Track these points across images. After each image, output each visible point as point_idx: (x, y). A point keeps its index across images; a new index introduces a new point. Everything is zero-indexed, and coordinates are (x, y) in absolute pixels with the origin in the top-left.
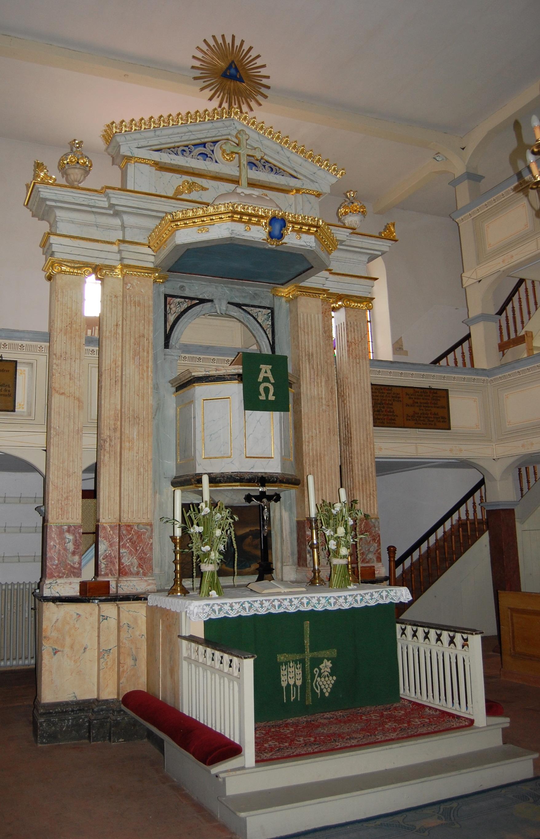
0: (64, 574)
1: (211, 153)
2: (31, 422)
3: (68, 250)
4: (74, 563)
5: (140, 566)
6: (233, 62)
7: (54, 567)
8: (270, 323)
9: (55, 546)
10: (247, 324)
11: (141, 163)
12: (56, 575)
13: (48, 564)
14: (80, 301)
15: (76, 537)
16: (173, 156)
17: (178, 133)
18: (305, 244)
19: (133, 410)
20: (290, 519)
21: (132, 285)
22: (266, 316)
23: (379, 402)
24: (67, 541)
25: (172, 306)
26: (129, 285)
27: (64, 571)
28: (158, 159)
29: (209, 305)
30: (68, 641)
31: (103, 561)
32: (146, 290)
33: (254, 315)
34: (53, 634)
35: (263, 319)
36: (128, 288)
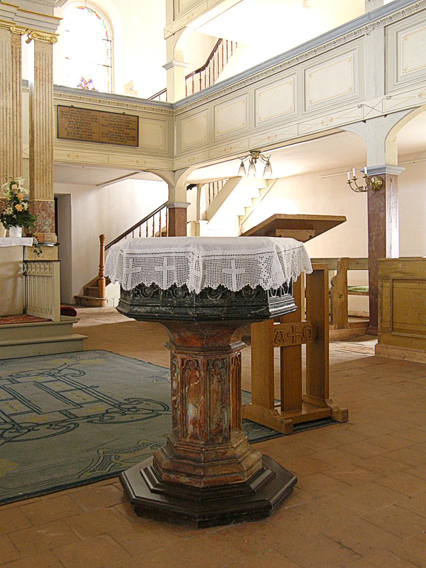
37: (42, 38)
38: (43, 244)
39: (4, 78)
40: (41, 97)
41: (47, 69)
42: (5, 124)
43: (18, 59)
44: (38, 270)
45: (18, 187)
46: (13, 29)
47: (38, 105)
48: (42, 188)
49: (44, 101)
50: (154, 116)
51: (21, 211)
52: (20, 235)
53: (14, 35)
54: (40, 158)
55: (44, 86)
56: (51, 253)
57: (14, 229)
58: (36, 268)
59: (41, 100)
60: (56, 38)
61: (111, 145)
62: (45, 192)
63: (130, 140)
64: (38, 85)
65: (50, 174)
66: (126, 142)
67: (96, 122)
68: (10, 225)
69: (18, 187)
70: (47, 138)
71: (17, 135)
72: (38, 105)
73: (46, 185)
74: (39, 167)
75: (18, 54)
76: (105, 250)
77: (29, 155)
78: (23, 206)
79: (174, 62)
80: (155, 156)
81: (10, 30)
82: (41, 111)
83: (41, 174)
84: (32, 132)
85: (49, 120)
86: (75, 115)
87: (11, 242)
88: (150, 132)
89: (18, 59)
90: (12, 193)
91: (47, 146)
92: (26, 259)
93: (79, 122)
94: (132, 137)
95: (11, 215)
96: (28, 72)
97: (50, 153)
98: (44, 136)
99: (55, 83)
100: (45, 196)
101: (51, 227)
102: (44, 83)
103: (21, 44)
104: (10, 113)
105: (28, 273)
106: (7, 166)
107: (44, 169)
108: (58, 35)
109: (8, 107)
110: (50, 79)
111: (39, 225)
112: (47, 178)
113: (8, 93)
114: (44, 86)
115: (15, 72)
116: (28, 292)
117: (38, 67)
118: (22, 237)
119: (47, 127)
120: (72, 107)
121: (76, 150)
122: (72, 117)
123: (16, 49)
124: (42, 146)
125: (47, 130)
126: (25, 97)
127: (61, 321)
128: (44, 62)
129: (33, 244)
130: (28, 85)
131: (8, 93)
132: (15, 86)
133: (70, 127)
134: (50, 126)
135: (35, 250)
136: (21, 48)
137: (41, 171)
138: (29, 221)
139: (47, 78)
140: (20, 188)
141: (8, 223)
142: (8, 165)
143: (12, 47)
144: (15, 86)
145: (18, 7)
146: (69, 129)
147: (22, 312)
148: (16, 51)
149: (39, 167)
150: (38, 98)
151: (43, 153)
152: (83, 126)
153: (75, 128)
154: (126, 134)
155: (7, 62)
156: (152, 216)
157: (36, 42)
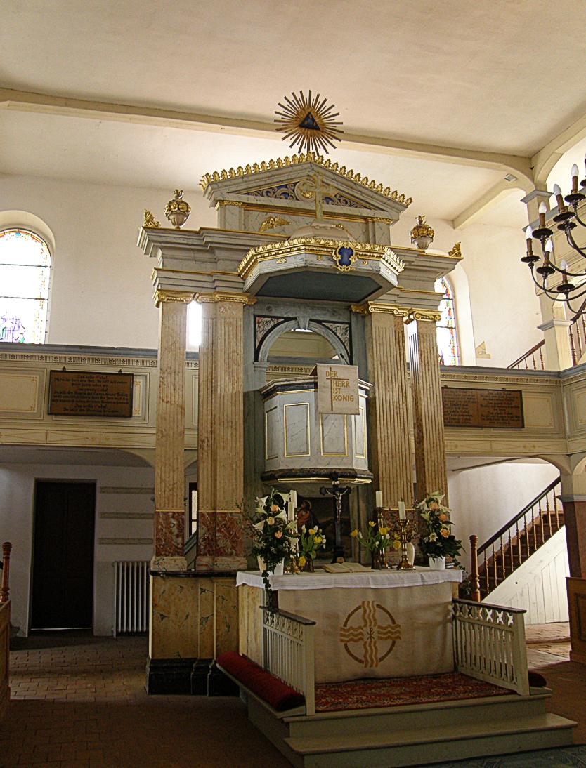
2: (146, 425)
3: (171, 282)
4: (178, 544)
5: (233, 547)
6: (310, 113)
10: (327, 338)
14: (212, 324)
15: (179, 522)
16: (259, 198)
17: (263, 178)
18: (371, 269)
19: (227, 416)
20: (367, 509)
22: (344, 331)
23: (455, 403)
29: (293, 322)
30: (173, 608)
31: (203, 543)
33: (334, 330)
34: (161, 602)
40: (428, 383)
50: (539, 389)
54: (431, 457)
59: (428, 388)
61: (492, 429)
63: (513, 420)
64: (424, 371)
65: (443, 475)
66: (509, 423)
67: (473, 402)
71: (405, 432)
75: (401, 339)
76: (478, 555)
79: (555, 322)
80: (543, 438)
82: (429, 401)
85: (433, 406)
88: (535, 408)
89: (401, 345)
91: (438, 441)
94: (516, 417)
97: (442, 450)
108: (441, 312)
109: (395, 400)
112: (440, 482)
115: (399, 360)
119: (437, 419)
124: (432, 443)
125: (437, 424)
127: (531, 695)
137: (433, 473)
147: (452, 669)
150: (425, 386)
152: (459, 408)
154: (509, 414)
155: (392, 349)
156: (529, 509)
157: (421, 325)
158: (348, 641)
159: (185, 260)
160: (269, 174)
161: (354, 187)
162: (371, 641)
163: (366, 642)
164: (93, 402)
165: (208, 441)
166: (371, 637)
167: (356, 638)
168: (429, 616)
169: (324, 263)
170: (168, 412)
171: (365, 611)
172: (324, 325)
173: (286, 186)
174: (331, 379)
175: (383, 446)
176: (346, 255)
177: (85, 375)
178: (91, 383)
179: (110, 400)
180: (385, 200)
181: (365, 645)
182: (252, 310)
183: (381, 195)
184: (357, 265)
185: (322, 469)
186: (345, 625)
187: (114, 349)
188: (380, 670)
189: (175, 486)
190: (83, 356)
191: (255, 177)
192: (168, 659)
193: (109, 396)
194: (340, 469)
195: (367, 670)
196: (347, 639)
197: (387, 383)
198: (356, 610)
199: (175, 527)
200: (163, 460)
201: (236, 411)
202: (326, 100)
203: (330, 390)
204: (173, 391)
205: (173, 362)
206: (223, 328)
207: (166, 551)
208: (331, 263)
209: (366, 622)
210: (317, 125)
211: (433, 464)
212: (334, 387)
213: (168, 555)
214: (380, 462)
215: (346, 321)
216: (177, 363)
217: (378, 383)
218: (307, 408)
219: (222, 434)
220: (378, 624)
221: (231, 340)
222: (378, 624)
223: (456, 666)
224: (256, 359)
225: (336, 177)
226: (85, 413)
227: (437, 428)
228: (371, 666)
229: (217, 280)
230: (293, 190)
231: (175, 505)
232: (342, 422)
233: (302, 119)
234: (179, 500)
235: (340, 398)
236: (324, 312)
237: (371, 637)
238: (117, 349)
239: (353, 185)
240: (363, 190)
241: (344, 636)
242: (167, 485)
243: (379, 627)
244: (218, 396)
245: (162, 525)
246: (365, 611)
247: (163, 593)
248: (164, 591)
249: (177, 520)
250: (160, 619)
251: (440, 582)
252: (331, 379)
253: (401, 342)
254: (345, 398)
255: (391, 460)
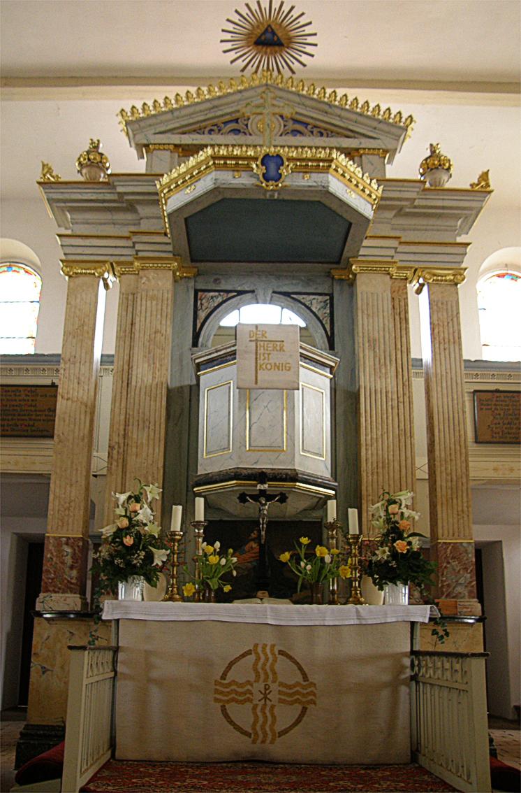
0: (60, 588)
1: (245, 127)
3: (79, 250)
7: (50, 581)
8: (328, 311)
9: (52, 559)
11: (159, 149)
12: (51, 589)
13: (43, 577)
15: (75, 550)
17: (201, 111)
18: (315, 184)
19: (144, 413)
21: (148, 279)
22: (322, 304)
23: (511, 412)
24: (65, 554)
25: (204, 301)
26: (145, 279)
27: (60, 585)
28: (177, 142)
32: (160, 282)
33: (307, 304)
34: (43, 651)
35: (318, 307)
36: (143, 282)
37: (439, 278)
38: (454, 618)
39: (382, 346)
40: (444, 368)
41: (450, 325)
42: (385, 416)
43: (403, 316)
44: (440, 672)
45: (400, 508)
46: (393, 270)
47: (439, 382)
48: (451, 520)
49: (449, 375)
51: (405, 552)
52: (405, 600)
53: (397, 281)
54: (446, 469)
55: (447, 352)
56: (468, 637)
57: (393, 590)
58: (435, 669)
59: (444, 373)
60: (461, 275)
62: (456, 526)
64: (437, 350)
65: (465, 495)
68: (384, 581)
69: (400, 508)
70: (457, 434)
72: (439, 382)
73: (458, 515)
74: (444, 484)
77: (427, 471)
78: (410, 543)
81: (389, 274)
82: (445, 391)
83: (449, 496)
84: (431, 450)
86: (504, 403)
87: (385, 615)
89: (403, 316)
90: (388, 521)
91: (458, 447)
92: (416, 648)
93: (510, 415)
95: (387, 562)
96: (422, 347)
97: (463, 459)
98: (452, 431)
99: (465, 357)
100: (456, 534)
101: (469, 588)
102: (447, 346)
103: (407, 293)
104: (392, 399)
105: (420, 679)
106: (389, 485)
107: (454, 487)
109: (389, 389)
110: (457, 338)
111: (448, 586)
113: (389, 368)
114: (447, 352)
115: (398, 336)
116: (422, 715)
117: (436, 322)
118: (409, 604)
119: (456, 415)
120: (497, 391)
121: (508, 459)
122: (498, 407)
123: (399, 301)
126: (418, 385)
128: (445, 314)
129: (431, 619)
130: (422, 366)
131: (389, 368)
132: (399, 356)
133: (496, 424)
134: (461, 414)
135: (434, 630)
136: (407, 298)
138: (422, 572)
139: (451, 337)
140: (404, 510)
141: (381, 578)
142: (391, 483)
143: (393, 299)
144: (399, 356)
145: (399, 238)
146: (494, 426)
148: (399, 305)
149: (444, 484)
151: (451, 460)
153: (504, 424)
158: (228, 701)
159: (101, 224)
160: (208, 105)
161: (330, 110)
162: (265, 704)
163: (257, 705)
164: (18, 420)
165: (119, 447)
166: (266, 698)
167: (240, 698)
168: (368, 673)
169: (243, 180)
170: (68, 411)
171: (258, 659)
172: (293, 298)
173: (236, 121)
174: (257, 340)
175: (370, 452)
176: (272, 166)
177: (10, 388)
178: (17, 398)
179: (39, 418)
180: (375, 124)
181: (255, 708)
182: (192, 284)
183: (368, 117)
184: (292, 180)
185: (246, 469)
186: (224, 677)
187: (44, 355)
188: (278, 749)
189: (72, 504)
190: (9, 367)
191: (191, 110)
192: (48, 726)
193: (38, 413)
194: (272, 469)
195: (257, 748)
196: (226, 698)
197: (377, 366)
198: (243, 656)
199: (69, 557)
200: (58, 471)
201: (157, 409)
202: (292, 8)
203: (254, 357)
204: (76, 385)
205: (79, 349)
206: (144, 302)
207: (55, 587)
208: (254, 181)
209: (258, 676)
210: (278, 39)
211: (449, 478)
212: (261, 351)
213: (58, 592)
214: (364, 474)
215: (326, 292)
216: (84, 351)
217: (364, 367)
218: (230, 388)
219: (135, 436)
220: (280, 679)
221: (154, 317)
222: (280, 679)
223: (415, 752)
224: (195, 344)
225: (304, 100)
226: (9, 433)
227: (457, 428)
228: (263, 742)
229: (138, 243)
230: (247, 125)
231: (70, 528)
232: (279, 403)
233: (259, 35)
234: (76, 522)
235: (269, 367)
236: (294, 282)
237: (266, 698)
238: (47, 355)
239: (326, 108)
240: (343, 114)
241: (222, 693)
242: (62, 503)
243: (281, 684)
244: (133, 388)
245: (52, 553)
246: (258, 659)
247: (47, 639)
248: (49, 637)
249: (72, 547)
250: (41, 672)
251: (389, 620)
252: (257, 340)
253: (403, 313)
254: (277, 367)
255: (380, 470)
